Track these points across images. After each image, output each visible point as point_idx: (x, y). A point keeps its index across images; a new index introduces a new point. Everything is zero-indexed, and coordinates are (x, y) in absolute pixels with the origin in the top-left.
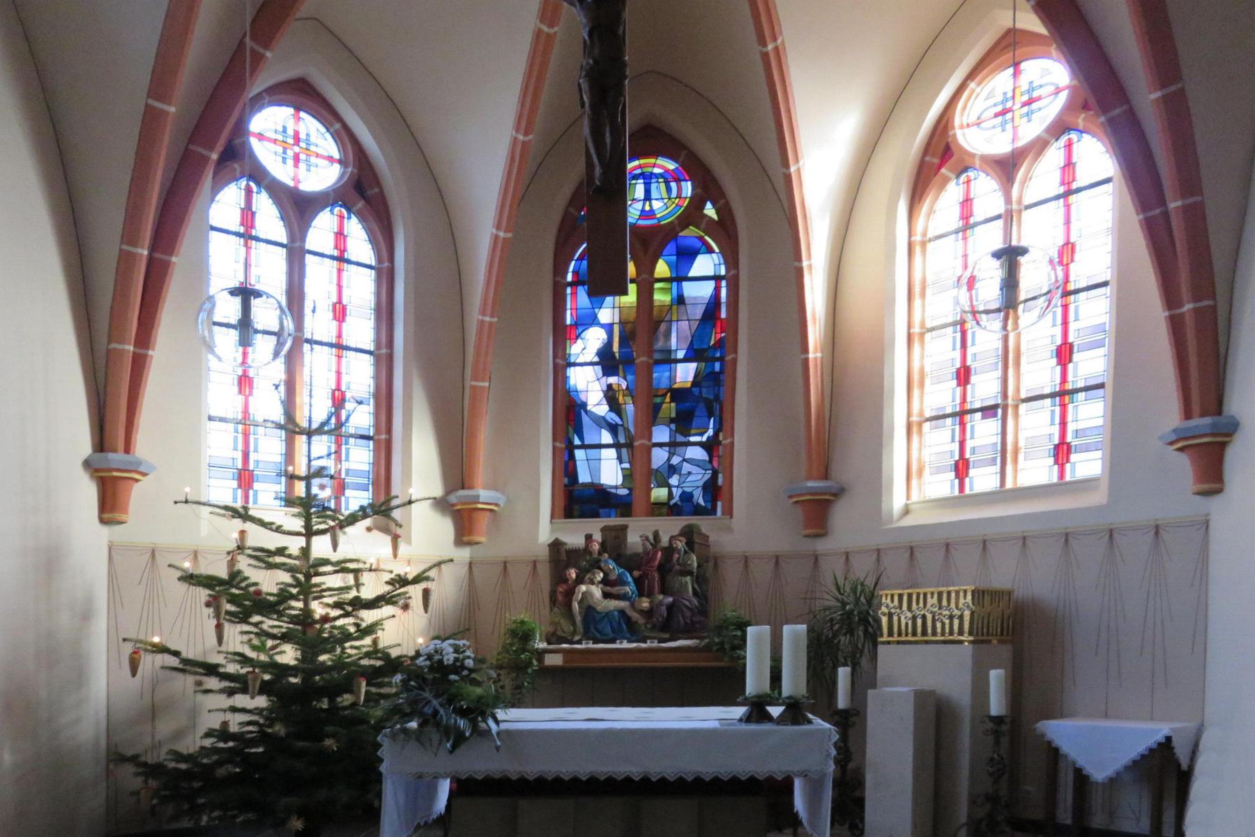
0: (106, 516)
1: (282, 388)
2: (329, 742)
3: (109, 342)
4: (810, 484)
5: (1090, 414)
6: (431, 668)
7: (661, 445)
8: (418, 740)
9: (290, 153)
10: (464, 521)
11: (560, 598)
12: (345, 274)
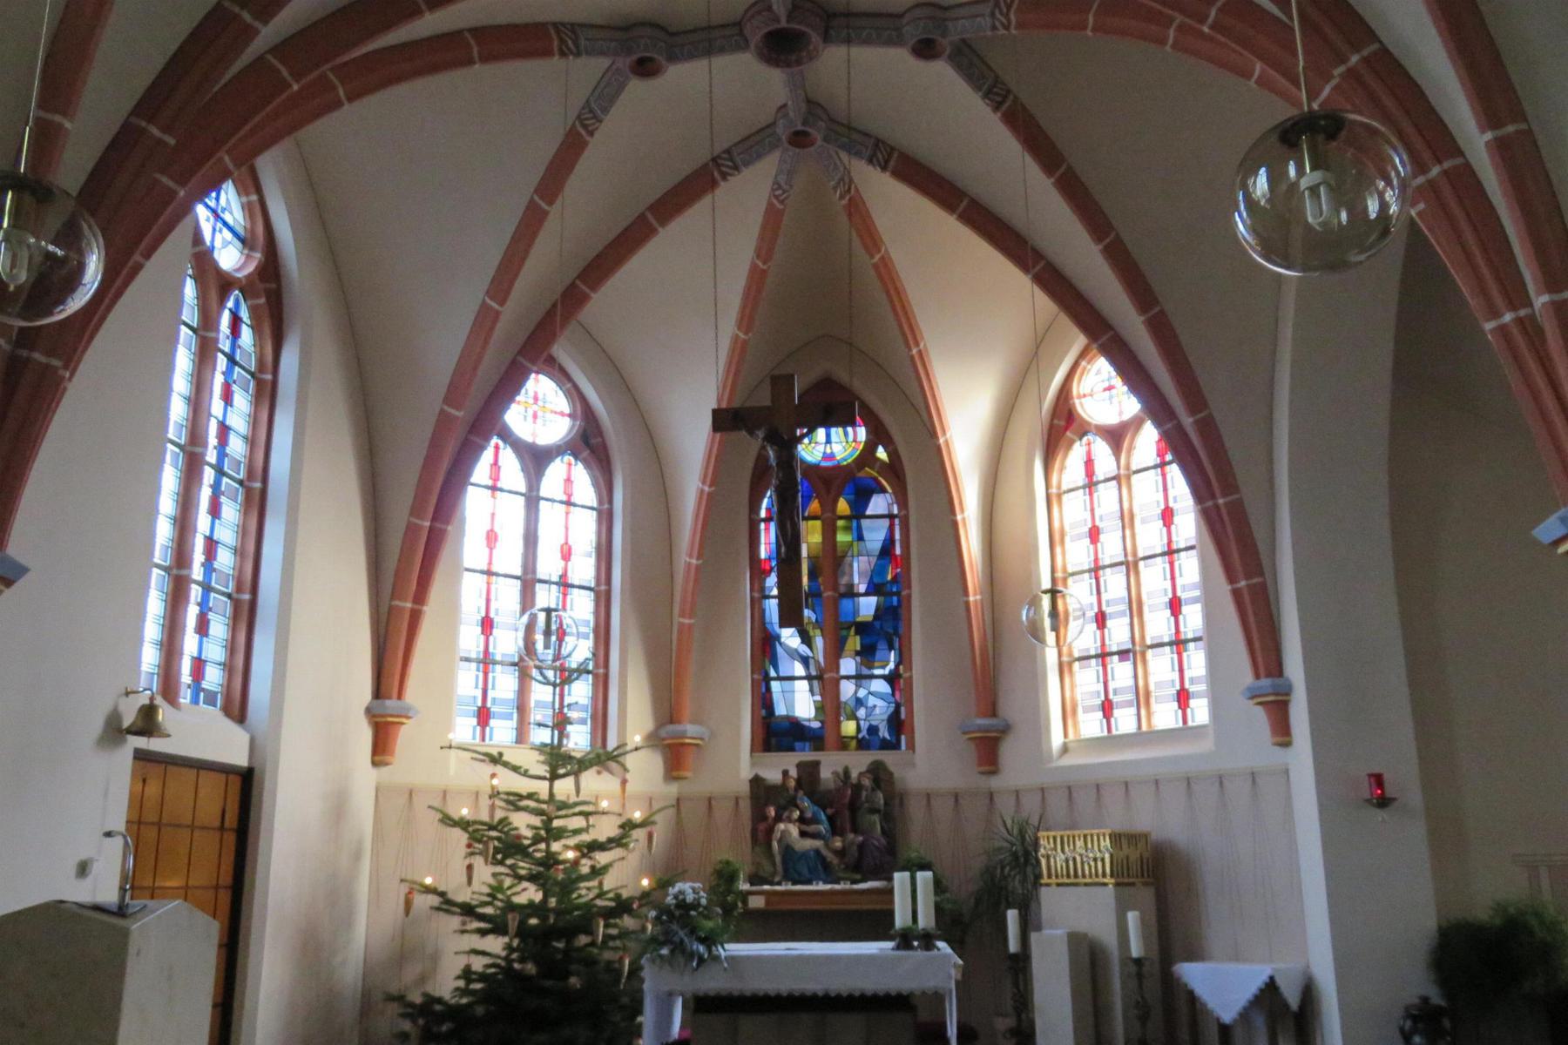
2: (573, 980)
3: (393, 597)
5: (1197, 661)
6: (678, 906)
7: (848, 678)
8: (671, 965)
9: (530, 413)
10: (675, 756)
12: (571, 516)
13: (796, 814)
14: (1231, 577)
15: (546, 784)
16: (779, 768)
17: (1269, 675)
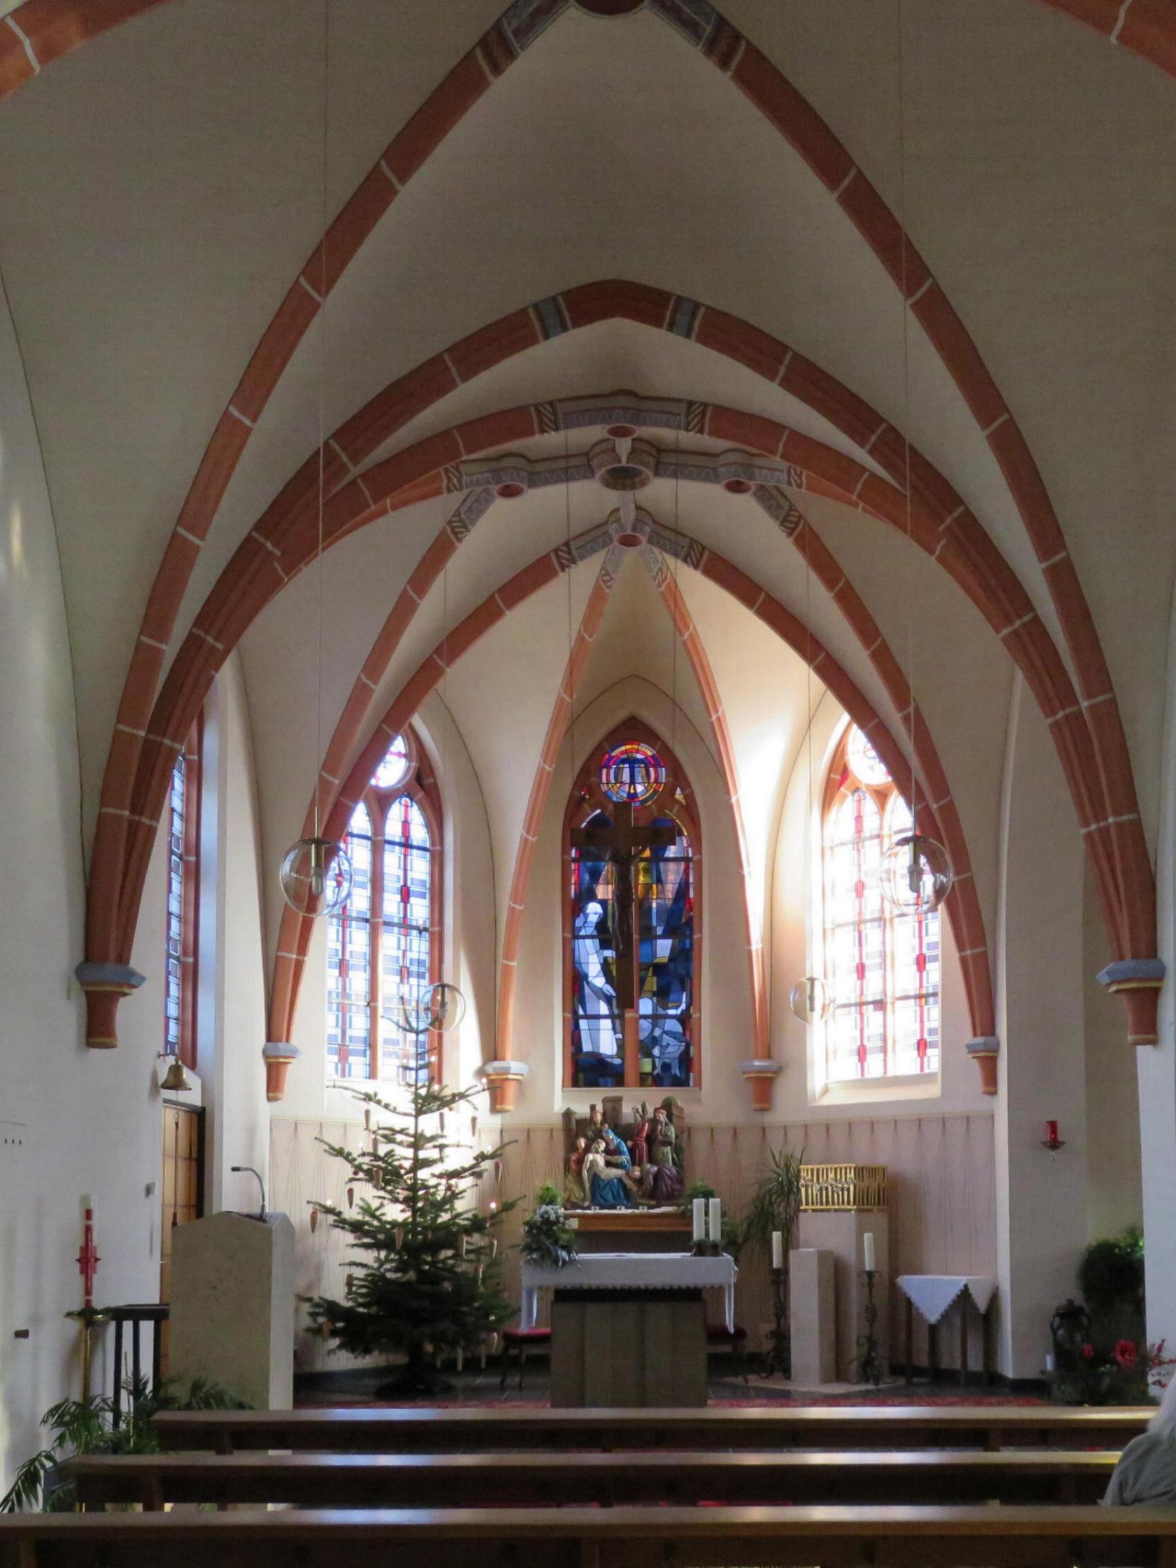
0: (91, 1040)
1: (368, 968)
3: (279, 949)
4: (757, 1063)
6: (542, 1223)
11: (573, 1165)
13: (603, 1146)
14: (961, 946)
15: (412, 1119)
16: (586, 1102)
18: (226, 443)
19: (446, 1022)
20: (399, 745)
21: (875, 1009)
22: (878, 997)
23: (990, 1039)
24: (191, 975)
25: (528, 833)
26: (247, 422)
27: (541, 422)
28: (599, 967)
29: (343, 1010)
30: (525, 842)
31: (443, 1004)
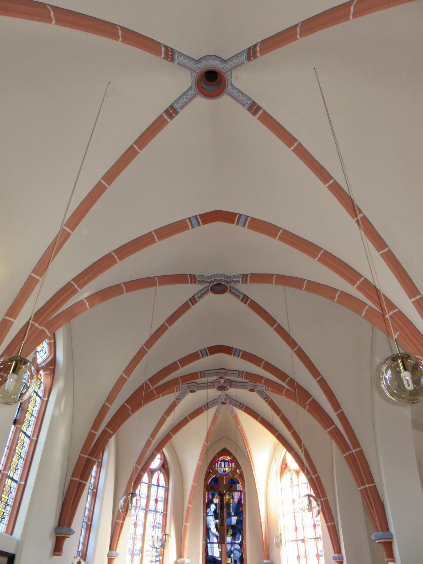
0: (56, 553)
3: (117, 519)
14: (327, 522)
17: (337, 553)
18: (121, 382)
19: (165, 547)
20: (158, 456)
21: (302, 542)
22: (302, 538)
23: (340, 555)
24: (89, 528)
25: (194, 482)
26: (126, 377)
27: (201, 376)
28: (214, 526)
29: (134, 539)
30: (193, 486)
31: (165, 541)
